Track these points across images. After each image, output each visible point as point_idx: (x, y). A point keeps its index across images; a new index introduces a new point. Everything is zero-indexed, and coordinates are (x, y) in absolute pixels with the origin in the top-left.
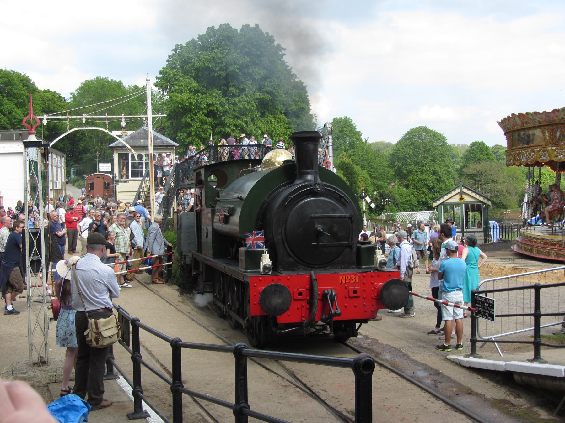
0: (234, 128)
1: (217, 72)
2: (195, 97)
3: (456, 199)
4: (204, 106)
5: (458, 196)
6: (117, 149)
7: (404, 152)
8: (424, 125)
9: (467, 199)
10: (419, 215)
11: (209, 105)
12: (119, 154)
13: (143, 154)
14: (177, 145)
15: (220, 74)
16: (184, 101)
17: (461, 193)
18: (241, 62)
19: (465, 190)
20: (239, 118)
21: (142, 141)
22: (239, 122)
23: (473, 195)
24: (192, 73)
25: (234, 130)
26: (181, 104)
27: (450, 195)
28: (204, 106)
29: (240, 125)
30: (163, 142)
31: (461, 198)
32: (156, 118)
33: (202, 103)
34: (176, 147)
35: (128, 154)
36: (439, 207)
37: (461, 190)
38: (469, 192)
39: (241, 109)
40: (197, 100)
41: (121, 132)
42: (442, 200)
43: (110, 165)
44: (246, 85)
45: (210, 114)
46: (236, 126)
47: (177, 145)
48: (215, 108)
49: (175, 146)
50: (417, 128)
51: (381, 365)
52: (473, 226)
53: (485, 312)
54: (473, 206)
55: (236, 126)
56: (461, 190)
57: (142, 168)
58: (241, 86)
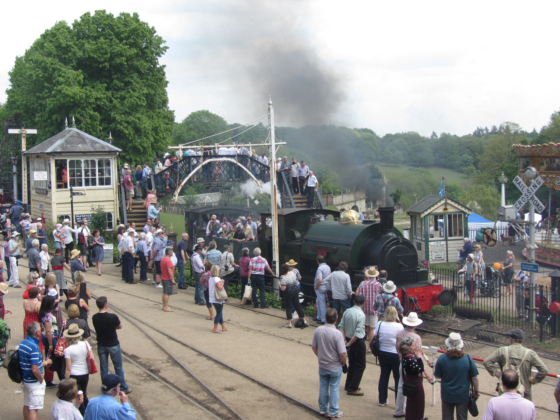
0: (126, 125)
1: (102, 63)
2: (84, 90)
3: (440, 210)
4: (93, 100)
5: (443, 207)
6: (54, 156)
7: (190, 135)
8: (206, 109)
9: (451, 210)
10: (207, 197)
11: (97, 99)
12: (56, 161)
13: (82, 160)
14: (120, 150)
15: (105, 66)
16: (76, 95)
17: (446, 204)
18: (128, 54)
19: (449, 202)
20: (129, 114)
21: (80, 145)
22: (131, 118)
23: (456, 205)
24: (72, 63)
25: (127, 127)
26: (73, 98)
27: (436, 206)
28: (93, 100)
29: (134, 121)
30: (103, 147)
31: (445, 209)
32: (268, 142)
33: (91, 97)
34: (120, 152)
35: (66, 160)
36: (426, 218)
37: (446, 201)
38: (453, 203)
39: (133, 105)
40: (86, 94)
41: (19, 130)
42: (429, 211)
43: (46, 173)
44: (132, 78)
45: (98, 109)
46: (127, 122)
47: (120, 150)
48: (102, 103)
49: (118, 151)
50: (199, 112)
51: (482, 393)
52: (455, 235)
53: (516, 323)
54: (455, 216)
55: (127, 122)
56: (446, 201)
57: (81, 176)
58: (127, 79)
